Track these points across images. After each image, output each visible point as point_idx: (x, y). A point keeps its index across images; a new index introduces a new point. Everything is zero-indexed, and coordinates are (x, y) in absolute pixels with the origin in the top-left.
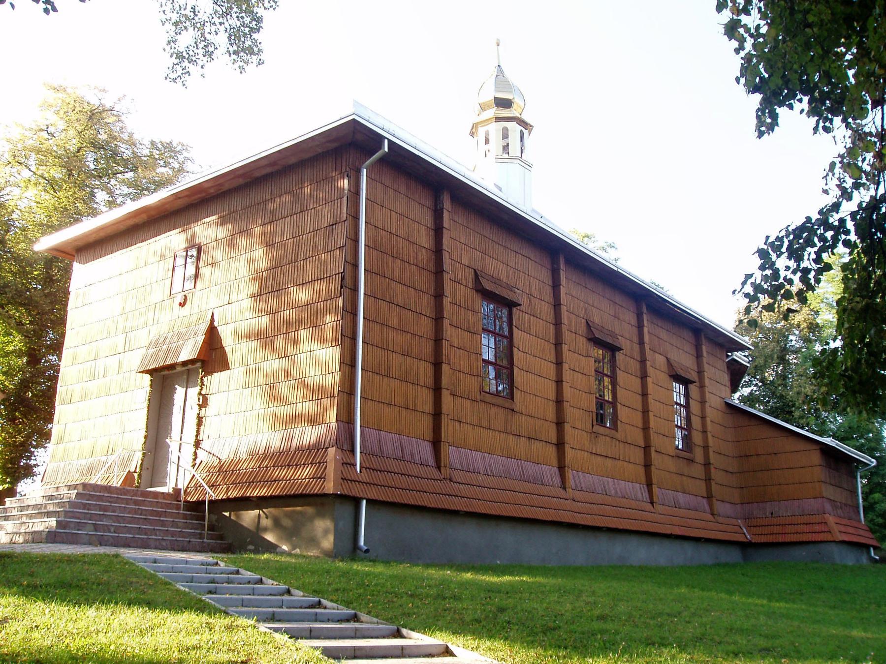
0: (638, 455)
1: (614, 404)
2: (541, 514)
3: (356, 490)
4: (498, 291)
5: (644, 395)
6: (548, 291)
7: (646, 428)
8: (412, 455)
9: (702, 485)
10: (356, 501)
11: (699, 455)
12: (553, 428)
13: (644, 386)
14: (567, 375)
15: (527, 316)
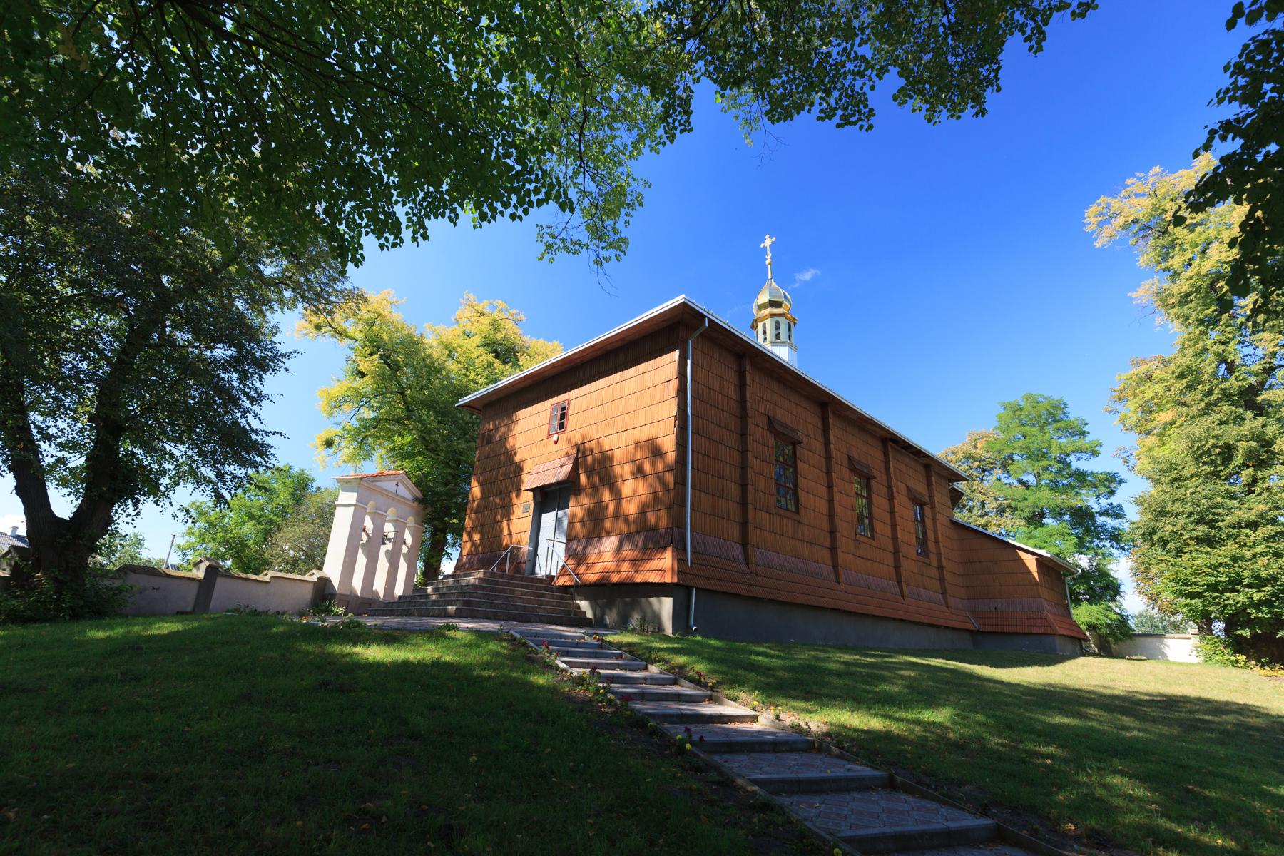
0: (889, 559)
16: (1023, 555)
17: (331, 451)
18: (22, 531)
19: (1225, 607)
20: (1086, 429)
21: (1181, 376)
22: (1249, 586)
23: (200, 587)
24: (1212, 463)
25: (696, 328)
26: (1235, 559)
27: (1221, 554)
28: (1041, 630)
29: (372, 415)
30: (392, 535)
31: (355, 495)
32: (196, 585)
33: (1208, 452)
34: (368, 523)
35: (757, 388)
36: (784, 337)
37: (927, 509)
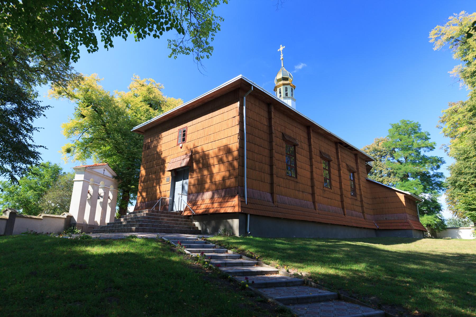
0: (338, 198)
8: (264, 198)
17: (70, 154)
30: (102, 194)
34: (91, 189)
36: (289, 95)
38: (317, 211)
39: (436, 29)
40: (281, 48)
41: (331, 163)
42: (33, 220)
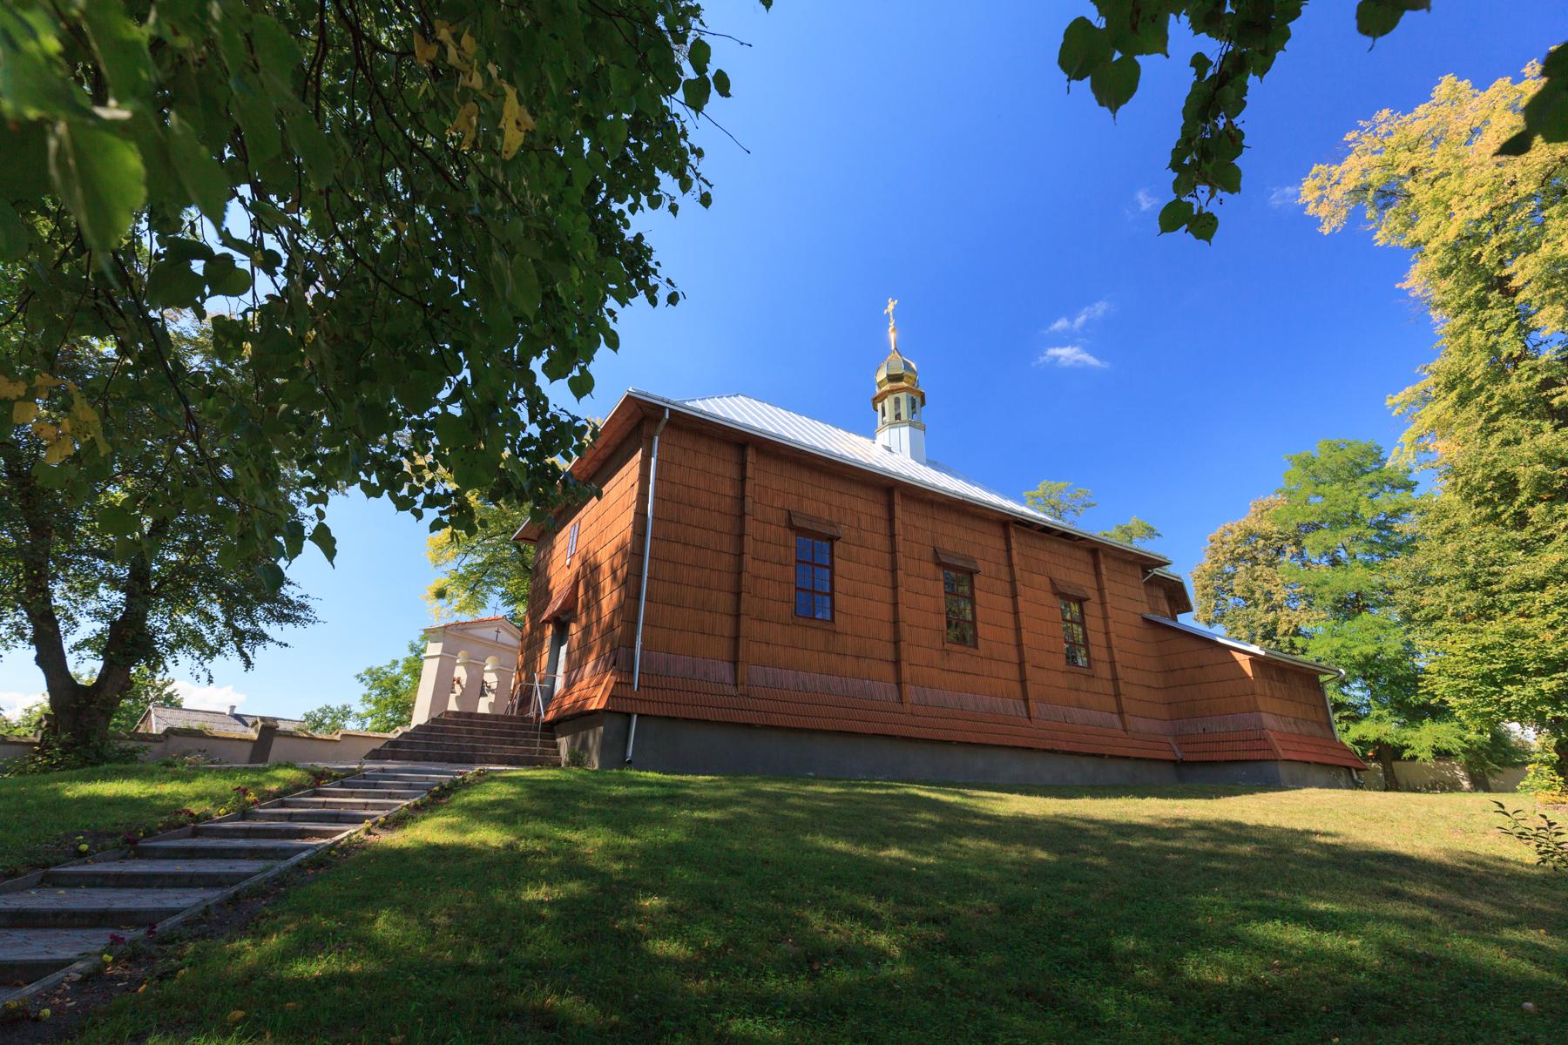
0: (1012, 672)
1: (973, 623)
2: (859, 727)
3: (625, 706)
4: (815, 527)
5: (1016, 613)
6: (882, 526)
7: (1019, 645)
8: (706, 674)
9: (1112, 701)
10: (629, 715)
11: (1103, 670)
12: (890, 646)
13: (1015, 605)
14: (1112, 627)
15: (855, 549)
16: (1237, 655)
17: (445, 601)
18: (47, 705)
19: (1508, 705)
20: (1412, 478)
21: (1451, 386)
22: (1539, 672)
23: (254, 749)
24: (1489, 502)
25: (658, 421)
26: (1514, 635)
27: (1494, 630)
28: (1257, 756)
29: (480, 560)
30: (494, 686)
31: (440, 645)
32: (250, 746)
33: (1480, 489)
34: (460, 672)
35: (761, 476)
36: (904, 416)
37: (1092, 608)
38: (908, 707)
39: (1317, 175)
40: (891, 307)
41: (976, 579)
42: (316, 743)
